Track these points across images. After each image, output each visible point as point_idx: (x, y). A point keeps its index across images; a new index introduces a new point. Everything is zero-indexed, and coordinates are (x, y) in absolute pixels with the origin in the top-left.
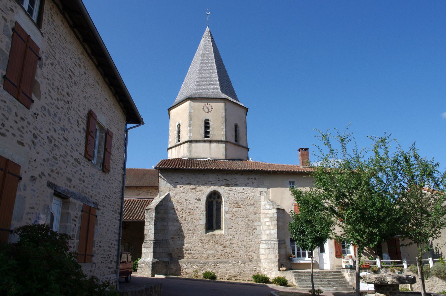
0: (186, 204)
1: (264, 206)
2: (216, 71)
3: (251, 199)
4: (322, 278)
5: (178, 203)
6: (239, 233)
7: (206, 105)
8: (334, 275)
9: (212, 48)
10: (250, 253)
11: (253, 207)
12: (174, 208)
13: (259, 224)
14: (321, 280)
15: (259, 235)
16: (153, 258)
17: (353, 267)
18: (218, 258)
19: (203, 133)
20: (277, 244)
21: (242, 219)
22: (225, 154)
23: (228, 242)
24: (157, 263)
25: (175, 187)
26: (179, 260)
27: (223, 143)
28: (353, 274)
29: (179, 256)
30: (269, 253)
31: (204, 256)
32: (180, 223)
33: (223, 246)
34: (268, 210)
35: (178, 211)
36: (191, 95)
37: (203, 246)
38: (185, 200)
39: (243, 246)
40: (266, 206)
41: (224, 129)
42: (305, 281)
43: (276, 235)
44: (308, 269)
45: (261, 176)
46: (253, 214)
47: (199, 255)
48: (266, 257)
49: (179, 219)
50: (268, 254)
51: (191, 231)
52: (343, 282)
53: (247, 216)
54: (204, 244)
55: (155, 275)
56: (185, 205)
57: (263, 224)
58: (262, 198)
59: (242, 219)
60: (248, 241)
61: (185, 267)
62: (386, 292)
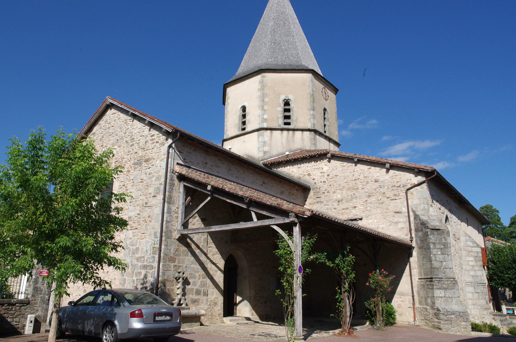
1: (465, 242)
40: (468, 243)
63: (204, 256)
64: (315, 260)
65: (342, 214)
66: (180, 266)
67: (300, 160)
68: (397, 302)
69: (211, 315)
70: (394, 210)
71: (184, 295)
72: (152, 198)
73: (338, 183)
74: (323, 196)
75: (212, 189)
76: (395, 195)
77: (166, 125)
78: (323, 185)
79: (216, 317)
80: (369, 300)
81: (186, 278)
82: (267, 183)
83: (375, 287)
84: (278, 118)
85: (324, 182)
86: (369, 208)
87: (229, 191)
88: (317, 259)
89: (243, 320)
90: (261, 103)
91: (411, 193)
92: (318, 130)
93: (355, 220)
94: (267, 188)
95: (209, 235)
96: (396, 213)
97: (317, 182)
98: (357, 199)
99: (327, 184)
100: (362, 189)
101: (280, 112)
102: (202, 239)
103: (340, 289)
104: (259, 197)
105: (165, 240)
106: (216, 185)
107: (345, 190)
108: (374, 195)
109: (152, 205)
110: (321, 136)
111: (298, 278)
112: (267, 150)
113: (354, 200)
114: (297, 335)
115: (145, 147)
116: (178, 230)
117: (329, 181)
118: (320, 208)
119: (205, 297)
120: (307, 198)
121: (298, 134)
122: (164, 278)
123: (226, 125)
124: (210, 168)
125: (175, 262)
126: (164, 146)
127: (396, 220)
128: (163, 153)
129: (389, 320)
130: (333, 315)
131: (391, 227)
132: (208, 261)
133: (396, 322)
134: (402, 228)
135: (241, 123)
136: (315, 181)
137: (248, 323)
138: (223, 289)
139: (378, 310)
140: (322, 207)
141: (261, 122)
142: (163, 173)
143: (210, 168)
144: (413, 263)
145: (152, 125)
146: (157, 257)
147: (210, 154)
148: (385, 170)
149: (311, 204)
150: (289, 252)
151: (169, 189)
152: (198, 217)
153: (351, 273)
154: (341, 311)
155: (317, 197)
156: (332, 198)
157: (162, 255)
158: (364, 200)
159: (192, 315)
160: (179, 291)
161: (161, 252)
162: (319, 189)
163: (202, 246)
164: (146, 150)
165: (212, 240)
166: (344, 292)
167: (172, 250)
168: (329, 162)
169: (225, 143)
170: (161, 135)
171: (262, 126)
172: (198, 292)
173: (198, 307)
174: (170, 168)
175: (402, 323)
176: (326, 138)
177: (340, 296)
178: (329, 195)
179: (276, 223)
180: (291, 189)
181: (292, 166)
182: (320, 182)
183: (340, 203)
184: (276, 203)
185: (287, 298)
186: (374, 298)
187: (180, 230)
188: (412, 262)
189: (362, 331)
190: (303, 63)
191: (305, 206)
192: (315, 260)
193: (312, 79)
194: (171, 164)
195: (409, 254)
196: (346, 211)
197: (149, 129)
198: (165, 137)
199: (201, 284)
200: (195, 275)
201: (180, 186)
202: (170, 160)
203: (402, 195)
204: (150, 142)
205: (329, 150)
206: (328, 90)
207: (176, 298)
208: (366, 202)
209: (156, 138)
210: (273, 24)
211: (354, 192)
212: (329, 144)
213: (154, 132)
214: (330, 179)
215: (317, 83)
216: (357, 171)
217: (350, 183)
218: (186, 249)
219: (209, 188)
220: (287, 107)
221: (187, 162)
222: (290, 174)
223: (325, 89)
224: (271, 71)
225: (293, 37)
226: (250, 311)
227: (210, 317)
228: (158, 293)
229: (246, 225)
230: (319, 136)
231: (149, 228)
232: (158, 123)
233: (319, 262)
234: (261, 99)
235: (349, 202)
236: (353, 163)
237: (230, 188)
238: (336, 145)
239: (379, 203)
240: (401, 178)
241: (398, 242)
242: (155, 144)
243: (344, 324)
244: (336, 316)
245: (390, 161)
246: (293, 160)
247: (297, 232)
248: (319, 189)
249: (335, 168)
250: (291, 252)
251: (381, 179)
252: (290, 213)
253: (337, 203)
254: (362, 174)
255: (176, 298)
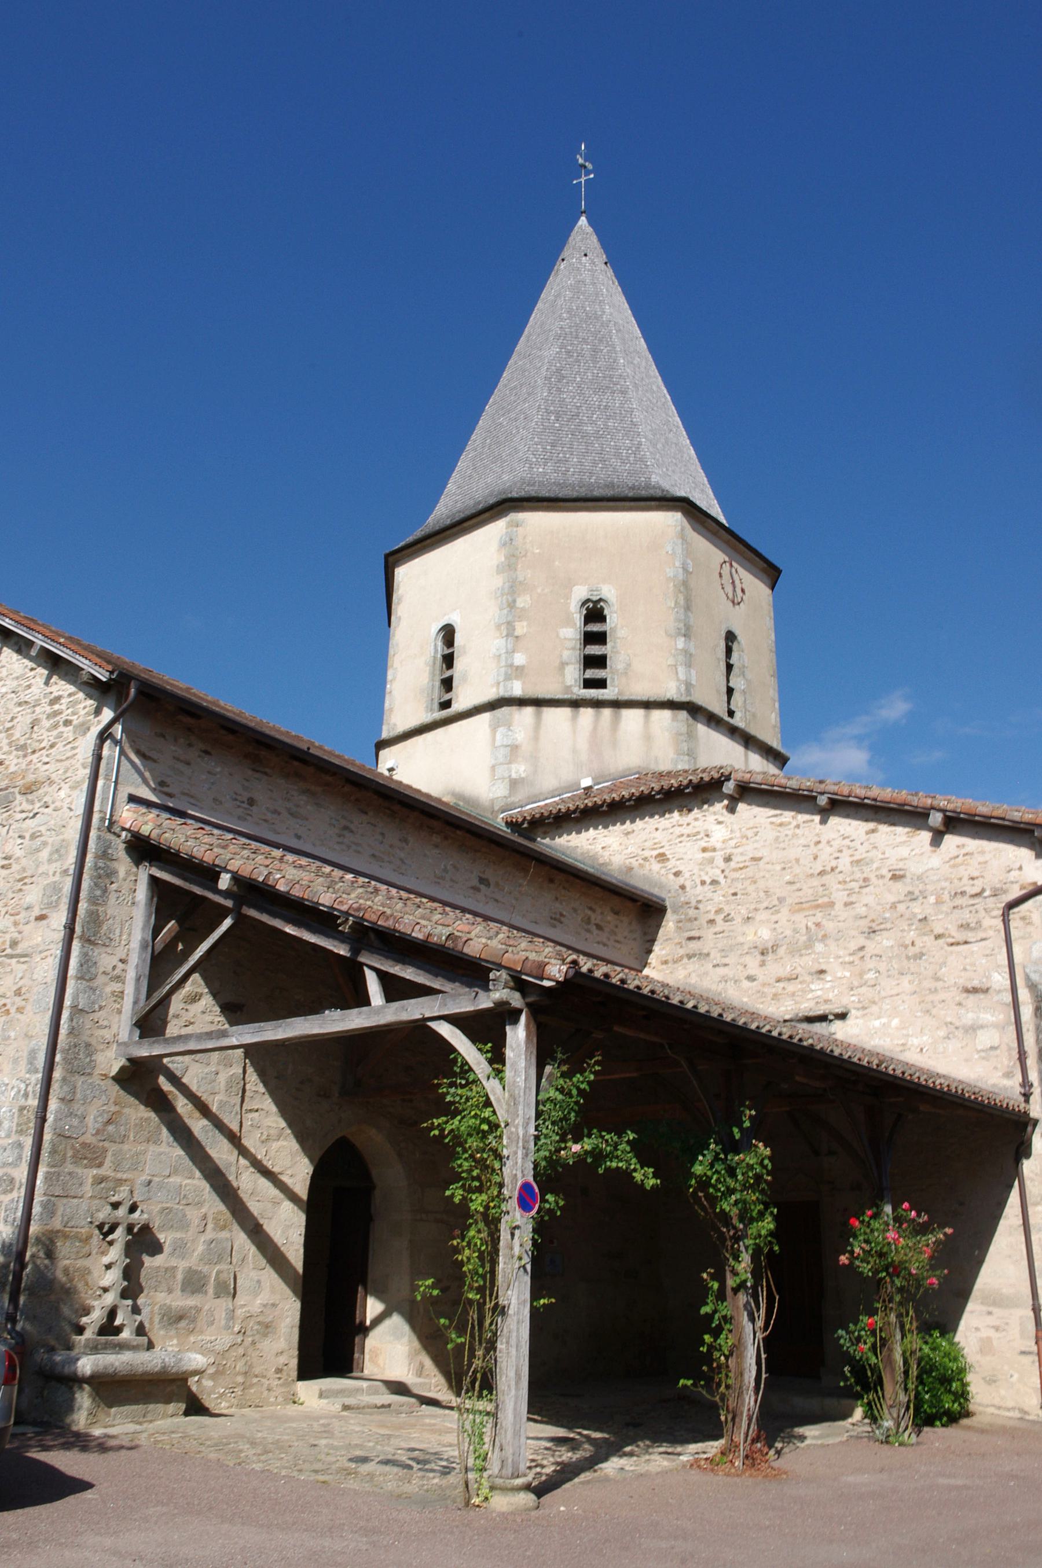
63: (225, 1144)
64: (589, 1160)
65: (775, 997)
66: (120, 1182)
67: (630, 806)
68: (977, 1329)
69: (243, 1370)
70: (961, 982)
71: (132, 1288)
72: (33, 924)
73: (762, 884)
74: (708, 933)
75: (235, 888)
76: (965, 927)
77: (91, 656)
78: (710, 895)
79: (263, 1380)
80: (856, 1324)
81: (146, 1229)
82: (497, 884)
83: (876, 1272)
84: (563, 665)
85: (714, 882)
86: (871, 975)
87: (288, 893)
88: (598, 1156)
89: (376, 1392)
90: (505, 611)
91: (1023, 918)
92: (704, 705)
93: (823, 1018)
94: (497, 901)
95: (252, 1064)
96: (967, 991)
97: (688, 884)
98: (828, 942)
99: (722, 889)
100: (846, 904)
101: (570, 644)
102: (222, 1078)
103: (721, 1278)
104: (389, 912)
105: (64, 1079)
106: (245, 872)
107: (785, 911)
108: (888, 925)
109: (30, 950)
110: (713, 724)
111: (517, 1232)
112: (523, 775)
113: (819, 947)
114: (504, 1472)
115: (29, 741)
116: (119, 1044)
117: (729, 881)
118: (699, 976)
119: (225, 1303)
120: (653, 941)
121: (632, 717)
122: (48, 1227)
123: (390, 692)
124: (266, 821)
125: (100, 1165)
126: (88, 734)
127: (969, 1018)
128: (81, 761)
129: (937, 1399)
130: (689, 1382)
131: (952, 1045)
132: (243, 1161)
133: (972, 1407)
134: (992, 1048)
135: (438, 684)
136: (681, 880)
137: (389, 1406)
138: (300, 1270)
139: (890, 1361)
140: (706, 973)
141: (501, 678)
142: (73, 833)
143: (266, 821)
144: (1032, 1180)
145: (54, 664)
146: (28, 1142)
147: (267, 770)
148: (926, 836)
149: (666, 962)
150: (485, 1127)
151: (91, 890)
152: (209, 996)
153: (761, 1215)
154: (719, 1366)
155: (690, 939)
156: (741, 939)
157: (47, 1137)
158: (853, 946)
159: (145, 1373)
160: (112, 1278)
161: (47, 1125)
162: (697, 908)
163: (220, 1108)
164: (30, 751)
165: (266, 1085)
166: (733, 1289)
167: (90, 1120)
168: (731, 810)
169: (383, 753)
170: (81, 695)
171: (506, 691)
172: (194, 1283)
173: (192, 1339)
174: (101, 811)
175: (996, 1412)
176: (734, 732)
177: (720, 1307)
178: (731, 928)
179: (446, 1013)
180: (591, 909)
181: (606, 827)
182: (698, 883)
183: (770, 957)
184: (446, 931)
185: (474, 1312)
186: (873, 1312)
187: (125, 1044)
188: (1031, 1175)
189: (823, 1446)
190: (654, 479)
191: (646, 972)
192: (589, 1160)
193: (683, 529)
194: (104, 800)
195: (1018, 1148)
196: (791, 987)
197: (45, 677)
198: (92, 702)
199: (209, 1249)
200: (185, 1215)
201: (136, 880)
202: (100, 783)
203: (991, 927)
204: (47, 724)
205: (729, 769)
206: (740, 570)
207: (95, 1303)
208: (861, 954)
209: (64, 707)
210: (557, 353)
211: (819, 917)
212: (746, 756)
213: (61, 687)
214: (735, 870)
215: (702, 545)
216: (828, 842)
217: (805, 887)
218: (153, 1115)
219: (224, 882)
220: (595, 627)
221: (170, 795)
222: (594, 857)
223: (731, 565)
224: (540, 504)
225: (624, 392)
226: (411, 1356)
227: (240, 1379)
228: (20, 1283)
229: (343, 1020)
230: (709, 726)
231: (12, 1034)
232: (68, 651)
233: (608, 1169)
234: (504, 601)
235: (801, 955)
236: (813, 814)
237: (292, 880)
238: (771, 759)
239: (908, 958)
240: (986, 862)
241: (969, 1100)
242: (61, 729)
243: (733, 1419)
244: (702, 1386)
245: (943, 804)
246: (605, 808)
247: (519, 1045)
248: (697, 908)
249: (750, 833)
250: (494, 1126)
251: (914, 868)
252: (491, 970)
253: (759, 958)
254: (846, 852)
255: (95, 1303)
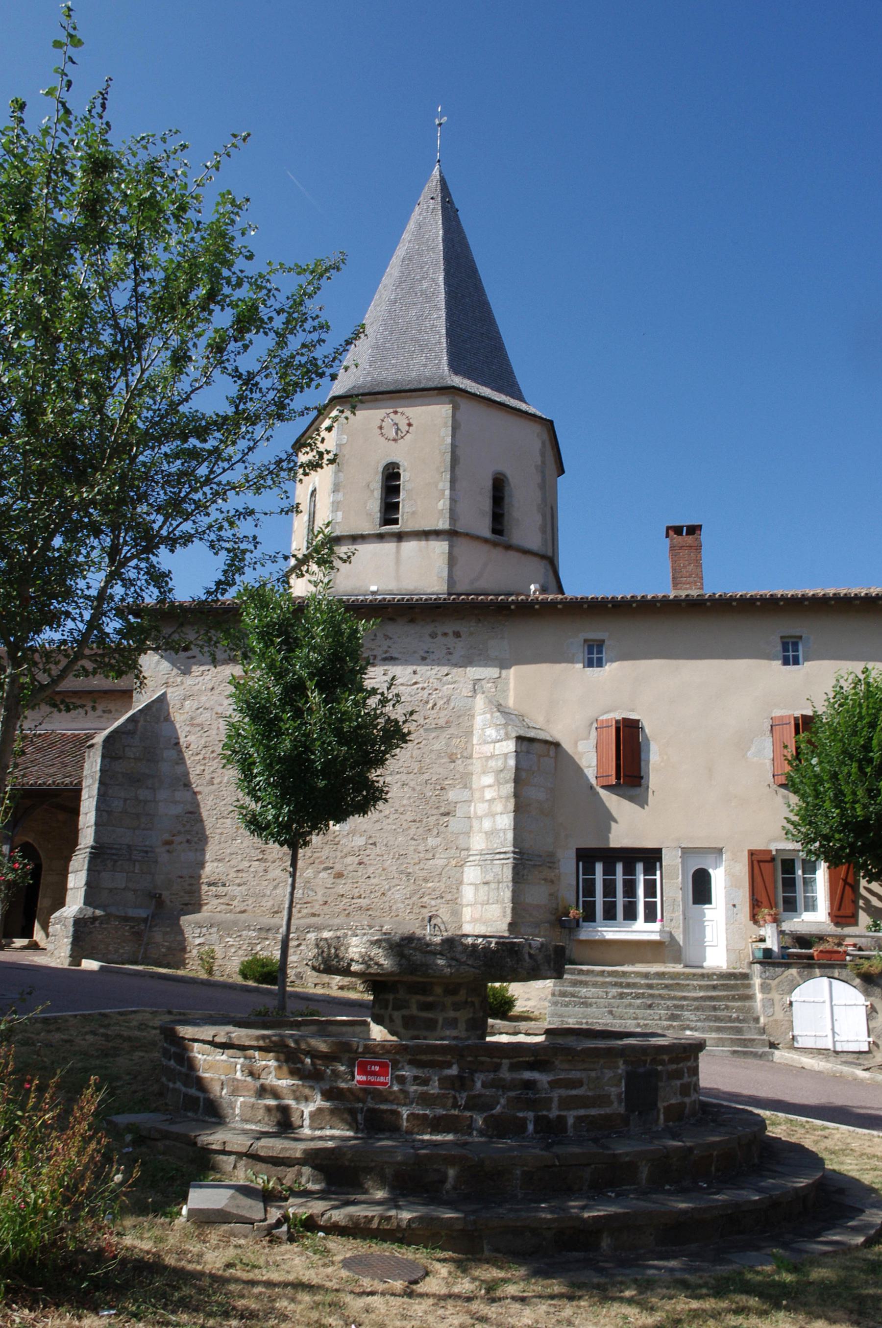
0: (218, 728)
1: (483, 729)
2: (442, 305)
3: (438, 707)
4: (660, 995)
5: (192, 725)
6: (389, 827)
7: (392, 415)
8: (714, 987)
9: (441, 232)
10: (425, 899)
11: (446, 734)
12: (178, 744)
13: (466, 795)
14: (649, 1002)
15: (462, 836)
16: (85, 904)
17: (775, 955)
18: (314, 915)
19: (378, 509)
20: (510, 866)
21: (404, 777)
22: (445, 574)
23: (349, 860)
24: (97, 924)
25: (186, 672)
26: (182, 918)
27: (442, 537)
28: (774, 983)
29: (186, 904)
30: (486, 898)
31: (268, 903)
32: (195, 793)
33: (334, 871)
34: (492, 745)
35: (190, 752)
36: (349, 390)
37: (266, 871)
38: (214, 716)
39: (401, 872)
41: (447, 492)
42: (582, 1003)
43: (510, 836)
44: (637, 965)
45: (480, 625)
46: (443, 761)
47: (250, 902)
48: (477, 916)
49: (193, 778)
50: (482, 904)
51: (228, 821)
52: (734, 1015)
53: (421, 768)
54: (267, 864)
55: (84, 961)
56: (215, 732)
57: (477, 795)
58: (480, 702)
59: (404, 777)
60: (422, 855)
61: (198, 941)
62: (392, 1020)
